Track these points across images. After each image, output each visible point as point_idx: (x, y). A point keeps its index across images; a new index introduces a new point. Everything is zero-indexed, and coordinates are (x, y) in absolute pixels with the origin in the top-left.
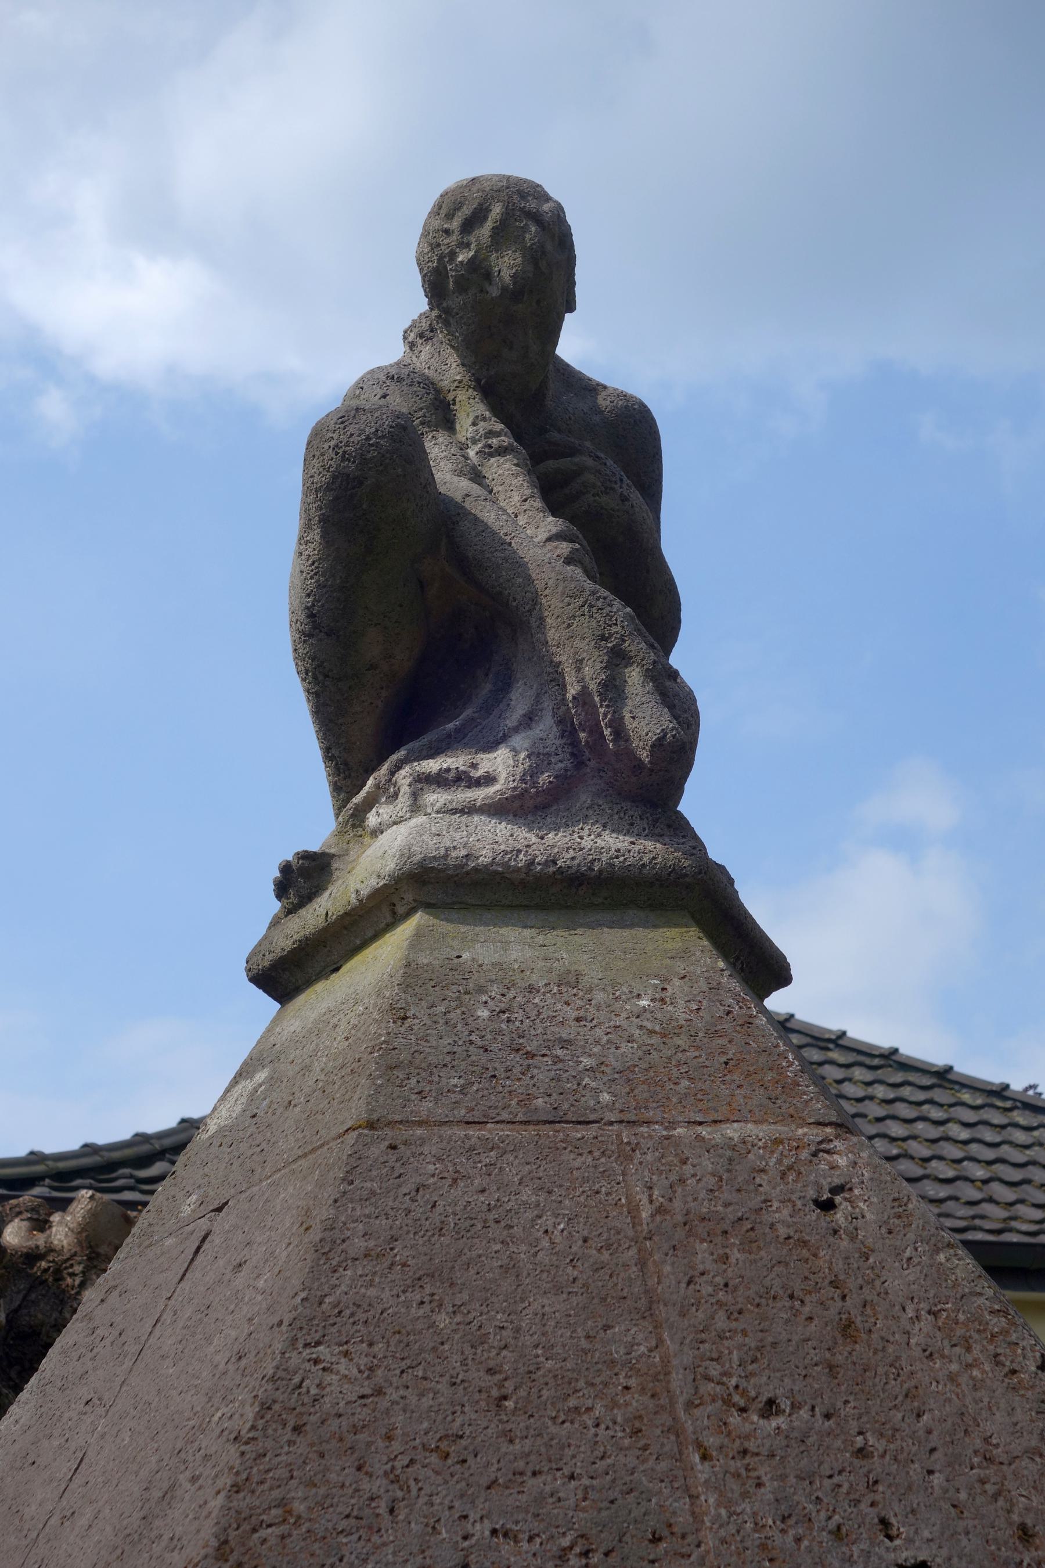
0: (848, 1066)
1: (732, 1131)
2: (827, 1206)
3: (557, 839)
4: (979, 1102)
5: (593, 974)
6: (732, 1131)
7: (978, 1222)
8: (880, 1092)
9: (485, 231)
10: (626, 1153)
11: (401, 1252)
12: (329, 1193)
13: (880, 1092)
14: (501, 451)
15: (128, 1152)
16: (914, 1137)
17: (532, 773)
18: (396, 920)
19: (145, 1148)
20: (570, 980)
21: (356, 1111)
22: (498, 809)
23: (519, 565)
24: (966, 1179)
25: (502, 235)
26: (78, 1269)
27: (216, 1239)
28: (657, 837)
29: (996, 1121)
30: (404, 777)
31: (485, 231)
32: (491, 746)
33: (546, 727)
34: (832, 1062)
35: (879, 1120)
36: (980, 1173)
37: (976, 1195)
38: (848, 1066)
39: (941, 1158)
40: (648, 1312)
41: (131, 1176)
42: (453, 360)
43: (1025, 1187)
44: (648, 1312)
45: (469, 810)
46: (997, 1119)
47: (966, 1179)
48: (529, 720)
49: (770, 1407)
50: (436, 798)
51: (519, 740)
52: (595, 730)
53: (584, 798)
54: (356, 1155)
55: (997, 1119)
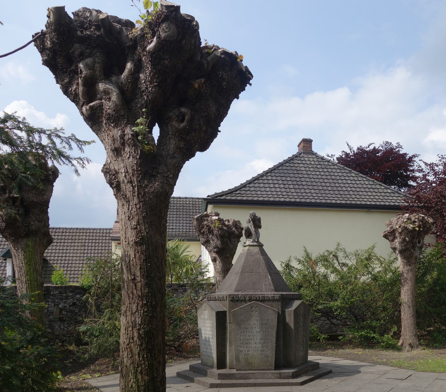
13: (340, 174)
19: (236, 189)
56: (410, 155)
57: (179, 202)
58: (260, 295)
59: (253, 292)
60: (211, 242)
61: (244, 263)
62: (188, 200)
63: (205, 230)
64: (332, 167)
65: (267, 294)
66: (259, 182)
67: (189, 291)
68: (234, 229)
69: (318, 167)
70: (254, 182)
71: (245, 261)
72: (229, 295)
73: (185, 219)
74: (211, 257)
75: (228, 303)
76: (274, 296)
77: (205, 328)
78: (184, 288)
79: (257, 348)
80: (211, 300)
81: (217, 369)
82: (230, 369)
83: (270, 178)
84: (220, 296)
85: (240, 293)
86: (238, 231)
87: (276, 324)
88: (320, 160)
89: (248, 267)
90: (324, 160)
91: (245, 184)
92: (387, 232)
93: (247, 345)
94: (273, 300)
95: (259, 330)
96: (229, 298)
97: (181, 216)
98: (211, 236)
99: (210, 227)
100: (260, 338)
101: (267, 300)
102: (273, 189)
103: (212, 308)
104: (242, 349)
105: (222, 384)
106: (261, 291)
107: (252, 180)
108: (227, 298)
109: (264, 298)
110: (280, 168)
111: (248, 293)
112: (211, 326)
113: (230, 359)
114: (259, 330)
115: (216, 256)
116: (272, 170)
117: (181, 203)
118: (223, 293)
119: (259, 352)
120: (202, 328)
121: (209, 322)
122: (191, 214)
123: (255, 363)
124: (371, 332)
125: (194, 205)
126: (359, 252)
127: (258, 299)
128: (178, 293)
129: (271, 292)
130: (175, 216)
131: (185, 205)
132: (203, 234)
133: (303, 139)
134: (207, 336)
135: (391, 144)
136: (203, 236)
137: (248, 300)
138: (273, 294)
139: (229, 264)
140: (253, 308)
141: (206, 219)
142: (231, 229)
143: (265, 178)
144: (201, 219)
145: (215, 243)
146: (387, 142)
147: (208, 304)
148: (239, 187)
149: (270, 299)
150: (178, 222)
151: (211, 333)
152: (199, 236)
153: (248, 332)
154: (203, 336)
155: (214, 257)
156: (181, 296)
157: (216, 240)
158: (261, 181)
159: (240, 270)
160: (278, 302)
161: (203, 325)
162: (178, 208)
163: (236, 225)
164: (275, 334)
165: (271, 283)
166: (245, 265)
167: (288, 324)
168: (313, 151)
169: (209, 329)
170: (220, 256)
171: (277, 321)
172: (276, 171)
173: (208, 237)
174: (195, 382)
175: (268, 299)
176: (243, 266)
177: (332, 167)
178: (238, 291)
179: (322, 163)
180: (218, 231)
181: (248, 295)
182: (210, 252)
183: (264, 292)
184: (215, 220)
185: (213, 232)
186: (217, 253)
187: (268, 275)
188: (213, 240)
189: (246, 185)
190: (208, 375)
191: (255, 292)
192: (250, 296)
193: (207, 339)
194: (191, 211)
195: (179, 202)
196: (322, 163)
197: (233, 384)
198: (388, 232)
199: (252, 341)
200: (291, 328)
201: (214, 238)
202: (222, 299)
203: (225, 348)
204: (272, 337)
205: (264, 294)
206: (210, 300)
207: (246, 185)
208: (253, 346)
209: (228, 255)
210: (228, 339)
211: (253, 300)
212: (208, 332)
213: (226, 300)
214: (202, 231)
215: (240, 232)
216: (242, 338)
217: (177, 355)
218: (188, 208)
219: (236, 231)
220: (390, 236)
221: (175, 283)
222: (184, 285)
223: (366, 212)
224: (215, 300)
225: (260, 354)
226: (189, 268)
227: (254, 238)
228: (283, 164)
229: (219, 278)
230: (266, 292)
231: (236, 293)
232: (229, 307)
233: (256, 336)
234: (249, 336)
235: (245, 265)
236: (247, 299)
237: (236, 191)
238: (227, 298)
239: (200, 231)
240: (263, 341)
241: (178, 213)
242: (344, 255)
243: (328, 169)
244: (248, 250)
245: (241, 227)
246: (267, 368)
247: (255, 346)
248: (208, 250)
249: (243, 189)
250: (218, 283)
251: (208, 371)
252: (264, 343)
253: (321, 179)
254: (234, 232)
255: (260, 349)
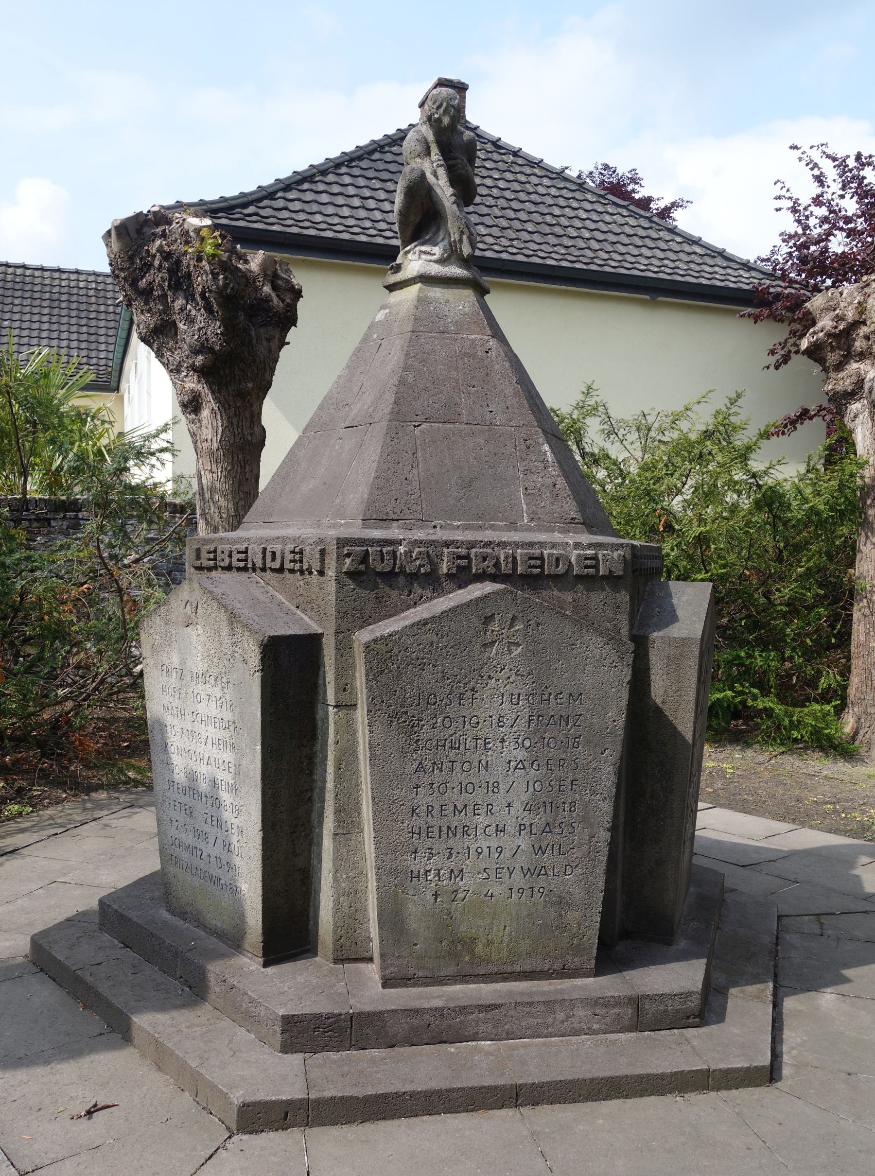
0: (541, 177)
1: (473, 336)
2: (487, 352)
3: (447, 269)
4: (594, 200)
5: (452, 300)
6: (473, 336)
7: (581, 258)
8: (553, 191)
9: (442, 110)
10: (455, 340)
11: (418, 356)
12: (406, 344)
13: (553, 191)
14: (441, 166)
15: (239, 201)
16: (563, 216)
17: (443, 254)
18: (415, 283)
19: (245, 199)
20: (447, 301)
21: (410, 328)
22: (436, 262)
23: (444, 207)
24: (581, 237)
25: (446, 112)
26: (261, 279)
27: (383, 347)
28: (466, 269)
29: (599, 210)
30: (417, 249)
31: (442, 110)
32: (435, 245)
33: (446, 242)
34: (535, 175)
35: (550, 206)
36: (587, 235)
37: (583, 245)
38: (541, 177)
39: (572, 227)
40: (457, 370)
41: (241, 213)
42: (431, 133)
43: (604, 243)
44: (457, 370)
45: (430, 261)
46: (600, 208)
47: (581, 237)
48: (443, 240)
49: (474, 386)
50: (424, 257)
51: (441, 245)
52: (456, 248)
53: (453, 260)
54: (411, 338)
55: (600, 208)
56: (662, 205)
57: (56, 282)
58: (516, 545)
59: (466, 528)
60: (182, 326)
61: (406, 368)
62: (82, 278)
63: (156, 277)
64: (528, 170)
65: (554, 545)
66: (314, 188)
67: (90, 527)
68: (267, 289)
69: (488, 166)
70: (300, 188)
71: (407, 355)
72: (339, 540)
73: (74, 329)
74: (180, 391)
75: (332, 587)
76: (595, 558)
77: (188, 725)
78: (72, 514)
79: (507, 854)
80: (215, 568)
81: (266, 965)
82: (336, 961)
83: (347, 180)
84: (278, 548)
85: (394, 532)
86: (283, 301)
87: (622, 721)
88: (489, 147)
89: (426, 389)
90: (500, 147)
91: (271, 190)
92: (821, 335)
93: (452, 842)
94: (589, 577)
95: (520, 754)
96: (340, 558)
97: (64, 320)
98: (180, 302)
99: (178, 262)
100: (525, 797)
101: (555, 578)
102: (362, 213)
103: (233, 618)
104: (418, 864)
105: (318, 1102)
106: (513, 526)
107: (292, 181)
108: (323, 560)
109: (542, 567)
110: (376, 156)
111: (441, 535)
112: (228, 716)
113: (337, 908)
114: (520, 754)
115: (199, 387)
116: (352, 160)
117: (63, 283)
118: (292, 531)
119: (518, 880)
120: (169, 720)
121: (217, 692)
122: (92, 315)
123: (490, 943)
124: (755, 691)
125: (102, 294)
126: (650, 419)
127: (504, 568)
128: (49, 532)
129: (562, 531)
130: (45, 319)
131: (75, 291)
132: (146, 294)
133: (439, 80)
134: (203, 769)
135: (614, 172)
136: (147, 303)
137: (449, 576)
138: (590, 546)
139: (252, 422)
140: (495, 626)
141: (159, 230)
142: (257, 289)
143: (331, 178)
144: (139, 232)
145: (200, 329)
146: (606, 167)
147: (205, 591)
148: (254, 197)
149: (576, 571)
150: (55, 335)
151: (227, 756)
152: (129, 305)
153: (457, 767)
154: (178, 761)
155: (192, 391)
156: (58, 543)
157: (200, 317)
158: (321, 187)
159: (386, 407)
160: (616, 589)
161: (176, 703)
162: (56, 296)
163: (275, 276)
164: (613, 778)
165: (561, 482)
166: (410, 379)
167: (659, 711)
168: (467, 122)
169: (212, 732)
170: (215, 387)
171: (624, 703)
172: (364, 164)
173: (167, 309)
174: (136, 1041)
175: (561, 569)
176: (402, 382)
177: (528, 170)
178: (385, 521)
179: (496, 156)
180: (215, 276)
181: (448, 544)
182: (174, 371)
183: (529, 529)
184: (198, 230)
185: (190, 285)
186: (203, 372)
187: (541, 438)
188: (190, 320)
189: (276, 192)
190: (212, 997)
191: (481, 528)
192: (463, 551)
193: (204, 786)
194: (94, 307)
195: (56, 282)
196: (496, 156)
197: (385, 1096)
198: (829, 335)
199: (482, 820)
200: (675, 733)
201: (193, 312)
202: (288, 565)
203: (311, 844)
204: (594, 793)
205: (542, 545)
206: (210, 569)
207: (276, 192)
208: (484, 843)
209: (250, 385)
210: (329, 796)
211: (481, 577)
212: (208, 751)
213: (321, 573)
214: (143, 284)
215: (288, 305)
216: (423, 800)
217: (45, 777)
218: (84, 299)
219: (275, 300)
220: (833, 349)
221: (40, 496)
222: (74, 506)
223: (642, 302)
224: (245, 569)
225: (521, 891)
226: (89, 448)
227: (455, 237)
228: (382, 147)
229: (209, 476)
230: (540, 529)
231: (377, 534)
232: (341, 614)
233: (503, 787)
234: (463, 788)
235: (410, 379)
236: (444, 568)
237: (245, 205)
238: (323, 560)
239: (134, 284)
240: (539, 820)
241: (56, 311)
242: (602, 427)
243: (517, 173)
244: (421, 300)
245: (293, 287)
246: (557, 966)
247: (494, 843)
248: (166, 365)
249: (265, 203)
250: (207, 496)
251: (214, 969)
252: (548, 828)
253: (501, 200)
254: (267, 300)
255: (522, 861)
